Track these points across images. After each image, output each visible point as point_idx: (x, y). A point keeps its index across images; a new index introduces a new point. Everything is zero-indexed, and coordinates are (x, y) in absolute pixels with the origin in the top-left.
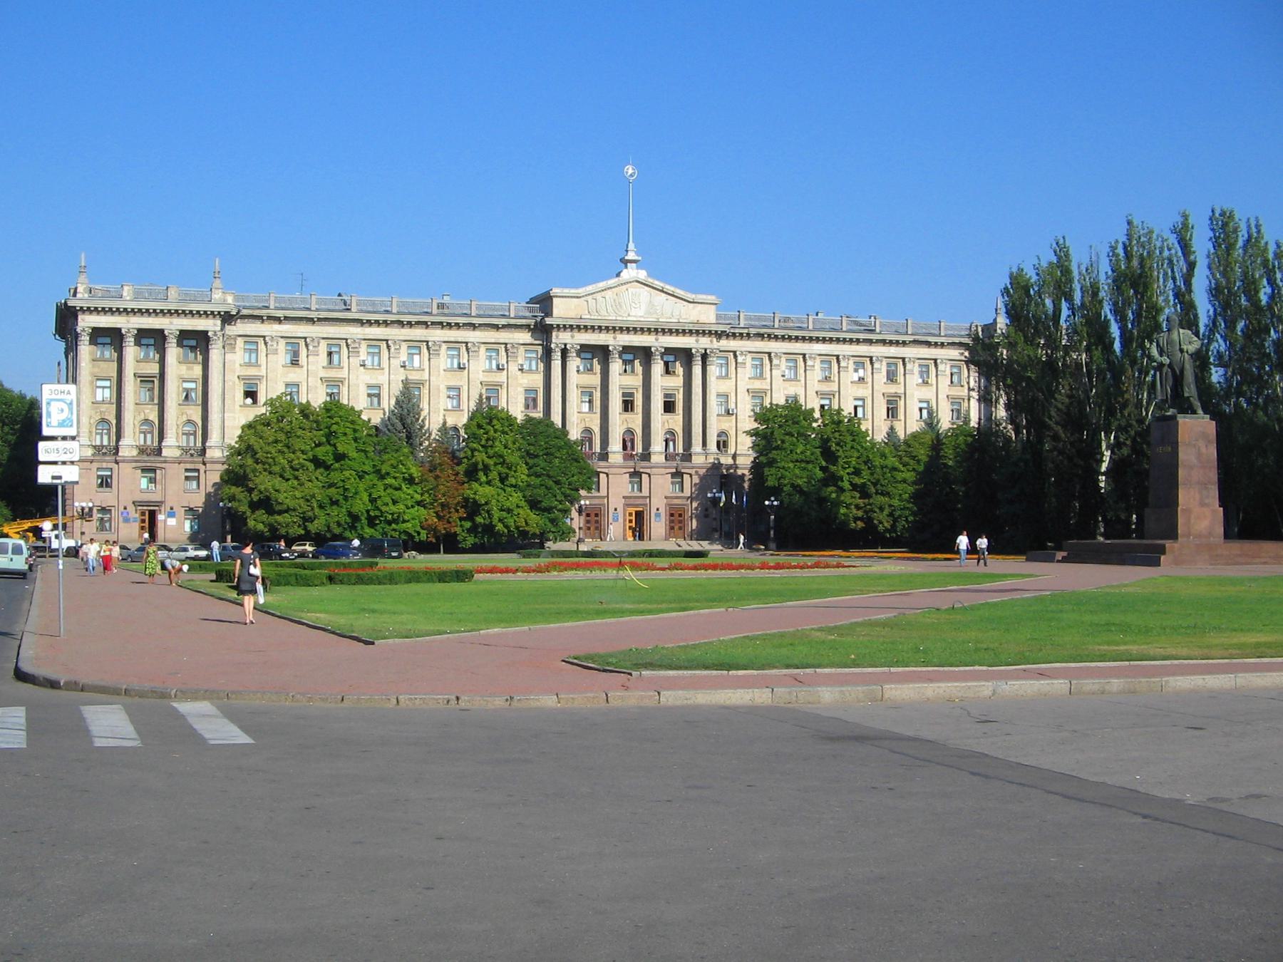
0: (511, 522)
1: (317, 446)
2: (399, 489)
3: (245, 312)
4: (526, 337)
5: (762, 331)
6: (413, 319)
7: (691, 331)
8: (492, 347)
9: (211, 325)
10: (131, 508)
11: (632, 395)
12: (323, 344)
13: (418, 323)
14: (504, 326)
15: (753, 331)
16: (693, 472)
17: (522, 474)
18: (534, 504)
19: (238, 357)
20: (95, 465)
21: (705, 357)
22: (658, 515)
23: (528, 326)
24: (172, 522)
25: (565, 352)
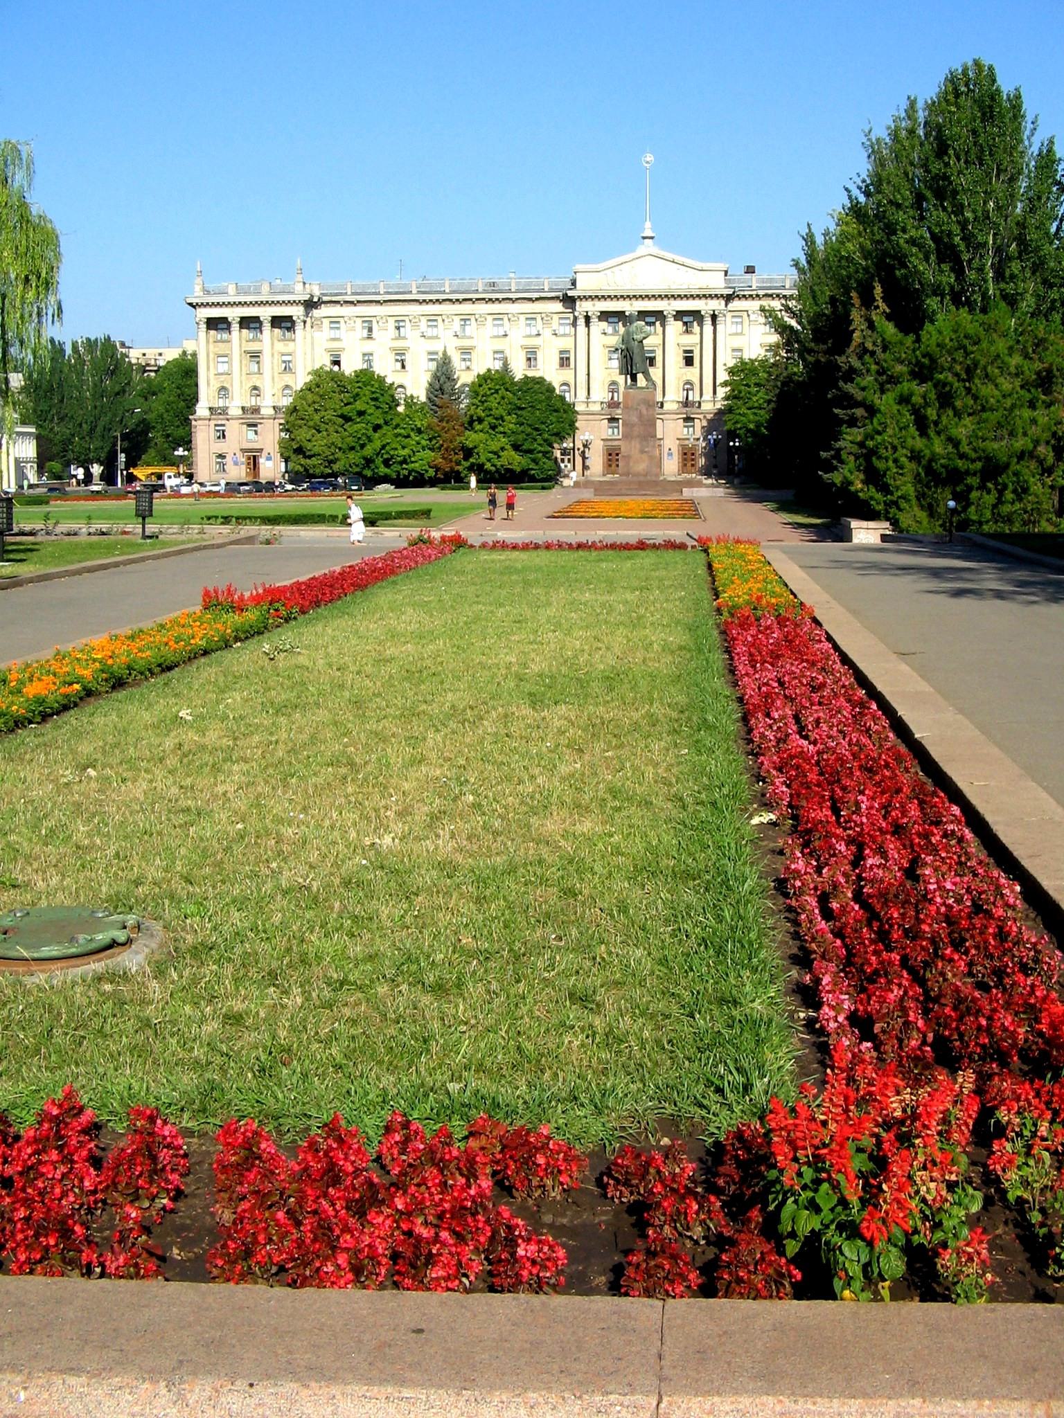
0: (496, 461)
1: (346, 405)
2: (408, 436)
3: (325, 299)
4: (558, 306)
5: (770, 292)
6: (461, 297)
7: (698, 296)
8: (531, 318)
9: (297, 312)
10: (239, 454)
11: (691, 352)
12: (391, 320)
13: (465, 300)
14: (537, 299)
15: (761, 293)
16: (701, 416)
17: (510, 423)
18: (516, 447)
19: (326, 332)
20: (213, 423)
21: (714, 317)
22: (670, 454)
23: (558, 298)
24: (270, 464)
25: (588, 319)
